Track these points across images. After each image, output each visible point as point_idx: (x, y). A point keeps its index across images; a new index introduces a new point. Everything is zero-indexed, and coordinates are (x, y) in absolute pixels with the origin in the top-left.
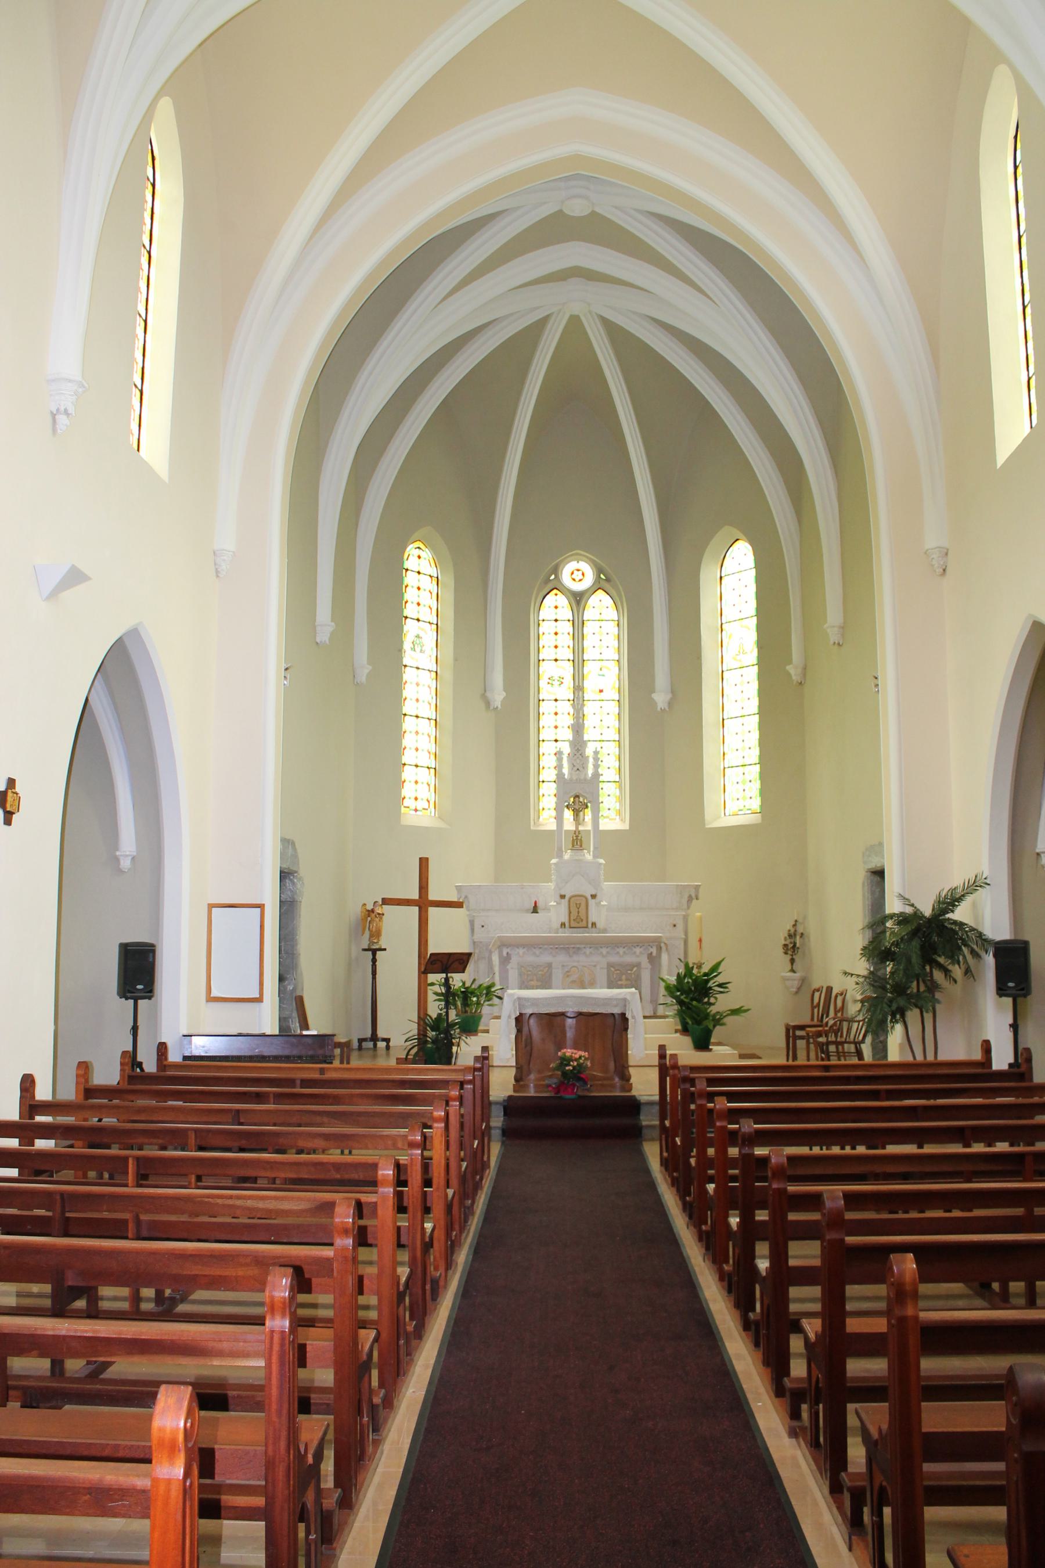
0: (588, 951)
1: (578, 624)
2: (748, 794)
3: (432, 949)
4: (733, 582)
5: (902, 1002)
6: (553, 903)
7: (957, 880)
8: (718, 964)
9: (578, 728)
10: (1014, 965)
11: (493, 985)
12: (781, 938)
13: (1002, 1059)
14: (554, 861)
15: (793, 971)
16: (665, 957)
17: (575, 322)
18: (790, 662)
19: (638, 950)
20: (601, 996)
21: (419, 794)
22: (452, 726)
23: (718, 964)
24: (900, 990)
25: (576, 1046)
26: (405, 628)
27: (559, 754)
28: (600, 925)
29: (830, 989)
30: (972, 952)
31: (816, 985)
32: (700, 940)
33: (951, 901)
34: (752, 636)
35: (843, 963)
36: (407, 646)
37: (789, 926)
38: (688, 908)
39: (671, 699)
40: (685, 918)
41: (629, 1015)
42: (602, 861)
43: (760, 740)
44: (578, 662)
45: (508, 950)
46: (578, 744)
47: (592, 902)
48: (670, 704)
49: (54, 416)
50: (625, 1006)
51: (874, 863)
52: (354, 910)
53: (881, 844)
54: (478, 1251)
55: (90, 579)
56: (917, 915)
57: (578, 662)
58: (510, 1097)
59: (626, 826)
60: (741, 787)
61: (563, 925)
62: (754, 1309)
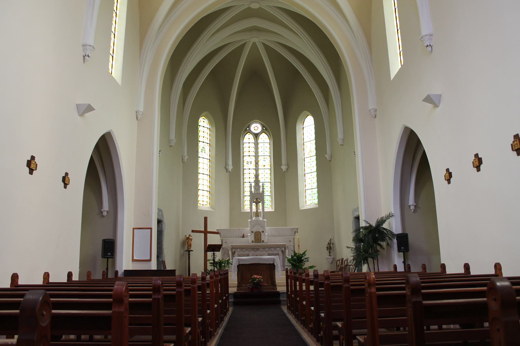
0: (261, 250)
1: (256, 144)
2: (314, 198)
3: (209, 243)
4: (307, 129)
5: (366, 255)
7: (383, 214)
8: (305, 252)
9: (257, 176)
10: (403, 241)
11: (229, 260)
12: (326, 244)
13: (401, 268)
15: (330, 256)
16: (287, 251)
17: (254, 44)
18: (326, 154)
19: (278, 249)
20: (266, 258)
21: (204, 199)
22: (214, 178)
23: (305, 252)
24: (366, 251)
26: (199, 145)
28: (266, 241)
29: (343, 259)
30: (389, 238)
31: (338, 259)
33: (382, 222)
34: (314, 146)
35: (346, 251)
36: (200, 150)
37: (328, 241)
40: (294, 239)
41: (275, 264)
43: (316, 143)
44: (257, 156)
46: (257, 181)
47: (262, 234)
48: (287, 169)
49: (84, 57)
51: (356, 214)
52: (182, 237)
53: (358, 208)
54: (226, 329)
55: (94, 109)
56: (371, 226)
57: (257, 156)
58: (236, 292)
59: (273, 210)
60: (311, 196)
62: (320, 333)
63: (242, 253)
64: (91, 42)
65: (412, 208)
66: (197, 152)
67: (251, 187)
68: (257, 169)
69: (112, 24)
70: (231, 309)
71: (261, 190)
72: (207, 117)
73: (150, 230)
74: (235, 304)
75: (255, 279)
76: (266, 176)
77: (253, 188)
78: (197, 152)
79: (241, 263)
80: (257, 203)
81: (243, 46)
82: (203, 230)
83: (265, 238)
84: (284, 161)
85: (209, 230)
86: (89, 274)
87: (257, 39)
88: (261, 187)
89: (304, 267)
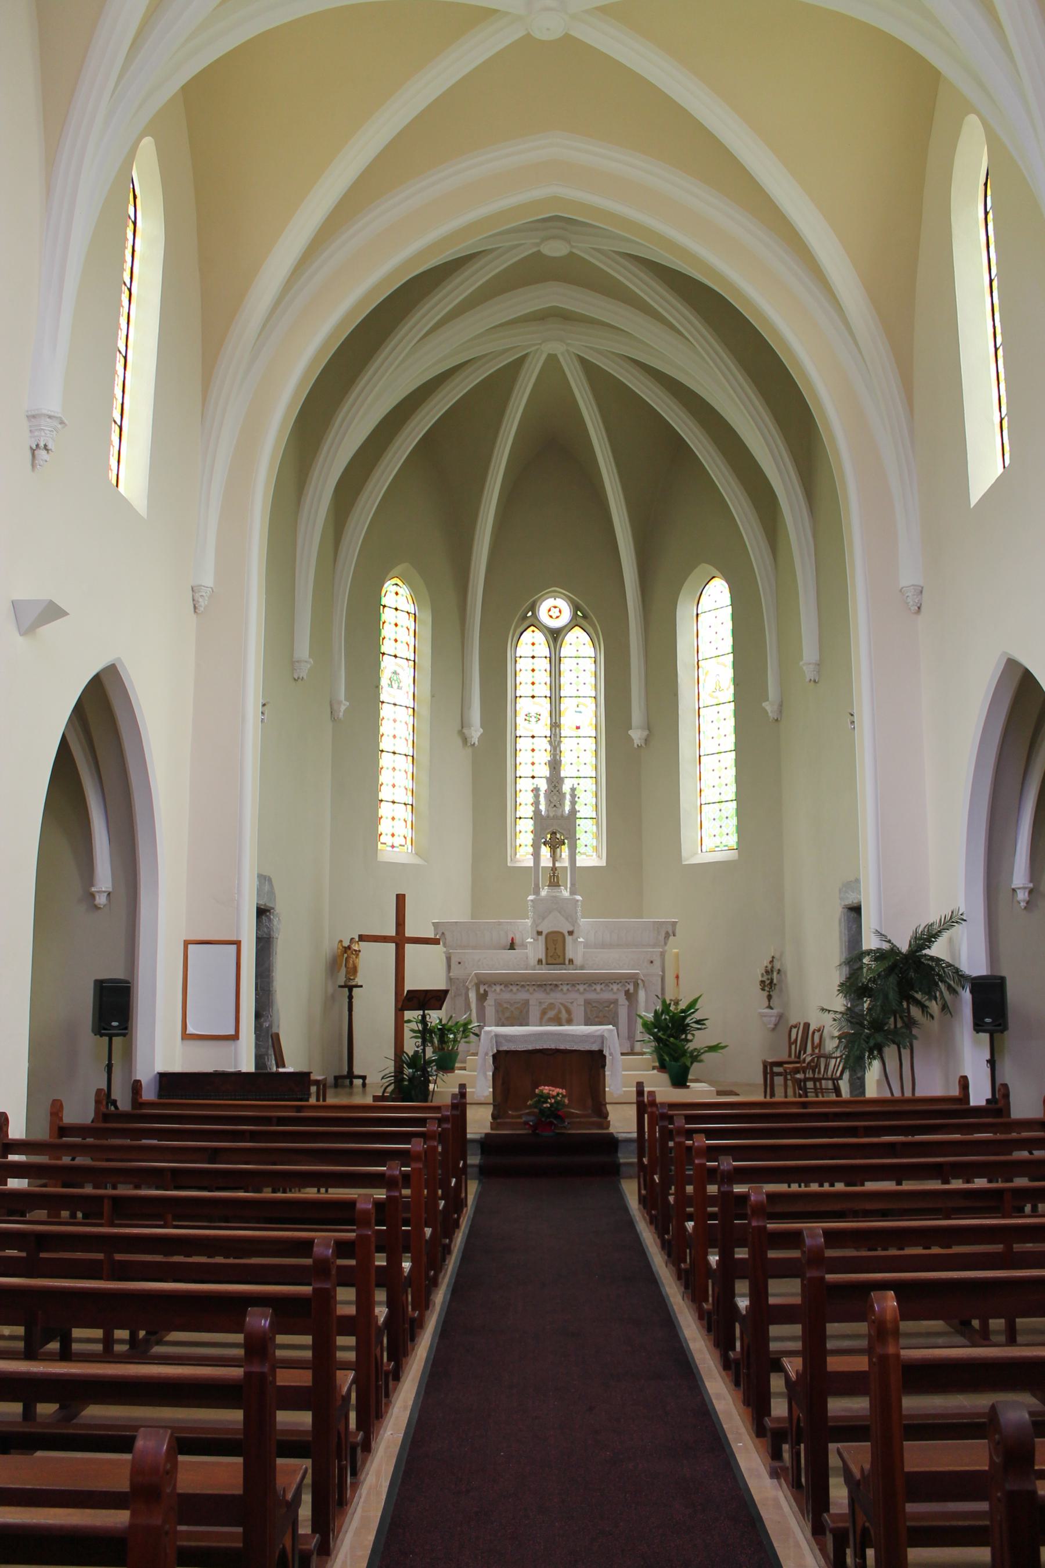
0: (565, 988)
1: (555, 661)
3: (409, 986)
4: (709, 620)
5: (879, 1038)
6: (529, 940)
7: (933, 916)
8: (695, 1001)
9: (555, 765)
10: (991, 1001)
12: (758, 974)
13: (979, 1095)
14: (531, 897)
15: (770, 1007)
16: (642, 994)
17: (552, 359)
19: (615, 987)
20: (579, 1033)
21: (396, 830)
22: (427, 763)
23: (695, 1001)
24: (877, 1026)
26: (383, 665)
27: (536, 791)
28: (578, 961)
29: (807, 1026)
31: (793, 1022)
32: (677, 977)
33: (928, 937)
34: (729, 673)
35: (820, 999)
36: (384, 682)
37: (766, 963)
38: (666, 944)
39: (648, 736)
40: (662, 954)
41: (606, 1052)
42: (579, 898)
44: (555, 698)
45: (486, 987)
46: (555, 780)
48: (647, 741)
49: (33, 451)
51: (851, 899)
52: (329, 947)
53: (857, 881)
54: (456, 1291)
56: (894, 951)
57: (555, 698)
58: (487, 1135)
59: (603, 863)
60: (717, 823)
64: (53, 405)
65: (1022, 896)
66: (377, 686)
69: (116, 372)
70: (472, 1189)
71: (567, 808)
73: (235, 946)
74: (485, 1172)
75: (545, 1098)
76: (583, 763)
77: (542, 799)
78: (377, 687)
80: (555, 845)
81: (516, 367)
82: (393, 933)
83: (575, 950)
84: (637, 715)
86: (56, 1109)
87: (562, 346)
88: (568, 797)
89: (690, 1046)
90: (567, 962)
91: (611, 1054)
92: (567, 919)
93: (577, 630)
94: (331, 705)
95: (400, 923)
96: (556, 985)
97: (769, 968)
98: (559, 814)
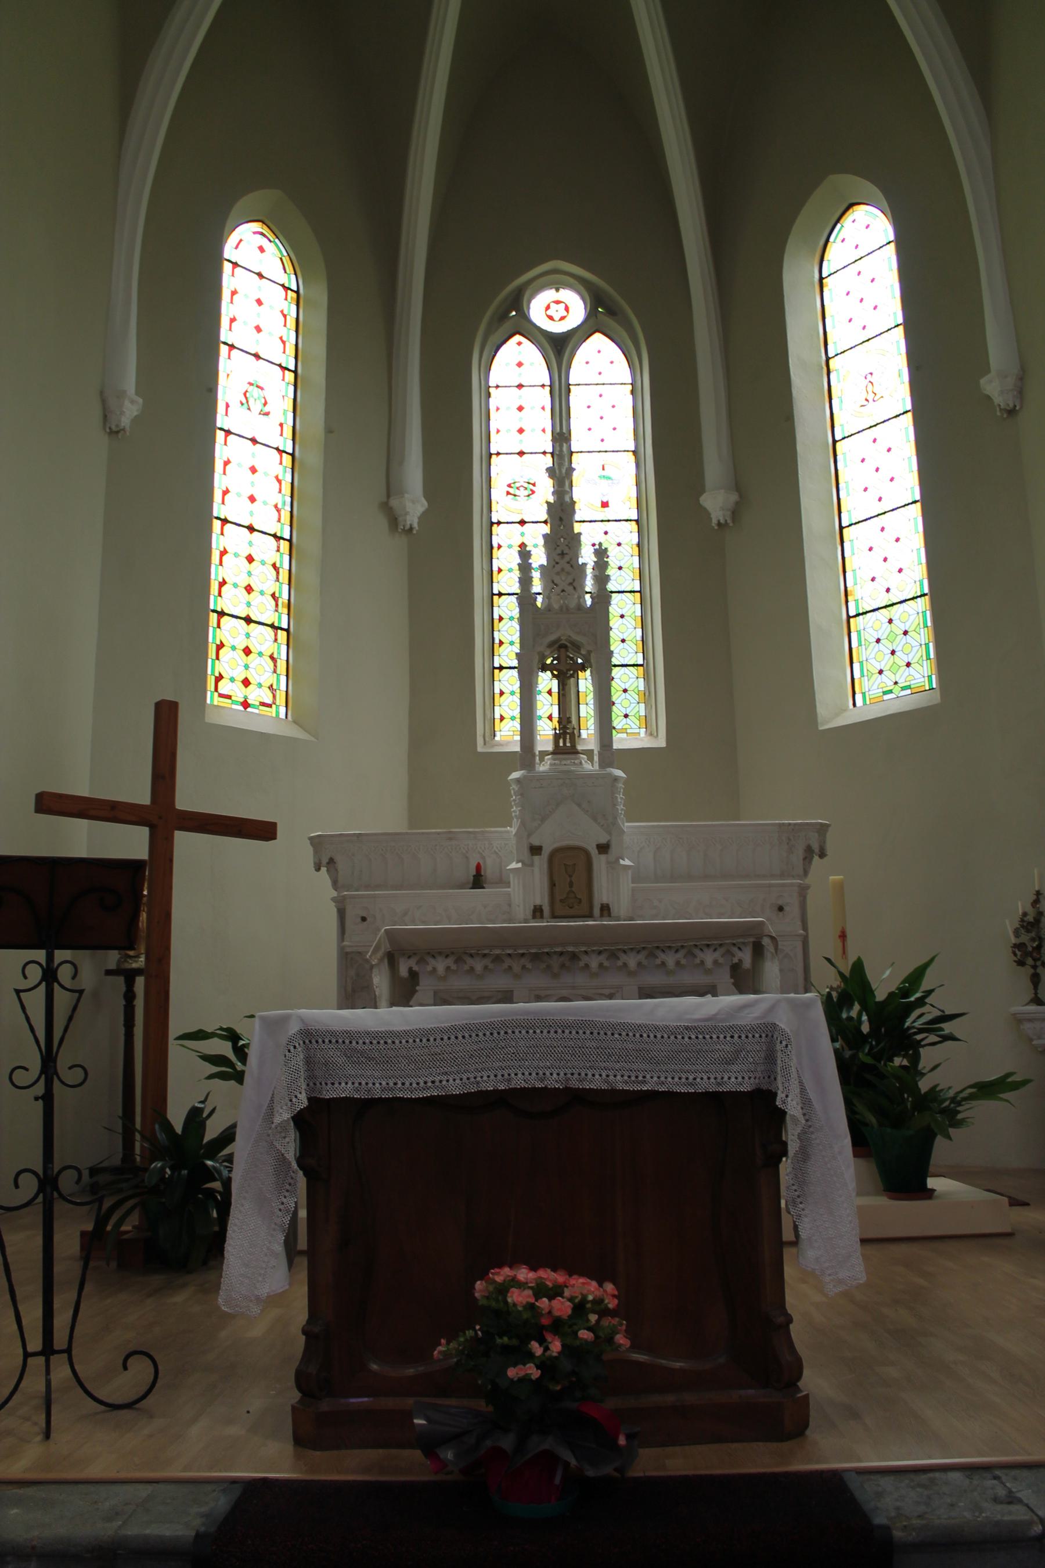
0: (594, 962)
1: (560, 392)
4: (856, 282)
6: (514, 865)
14: (515, 775)
15: (1037, 1001)
19: (709, 957)
20: (664, 1027)
23: (916, 977)
25: (616, 779)
27: (524, 553)
28: (622, 906)
32: (843, 936)
38: (806, 873)
39: (737, 503)
42: (619, 773)
45: (412, 963)
47: (600, 862)
48: (736, 513)
50: (770, 1058)
59: (661, 742)
61: (537, 912)
63: (460, 983)
67: (525, 568)
68: (561, 473)
72: (278, 226)
77: (536, 575)
79: (344, 1090)
82: (144, 798)
84: (714, 464)
85: (187, 798)
90: (597, 911)
91: (806, 1103)
92: (595, 819)
93: (598, 340)
94: (104, 402)
95: (164, 773)
96: (574, 957)
97: (1030, 918)
98: (573, 604)
